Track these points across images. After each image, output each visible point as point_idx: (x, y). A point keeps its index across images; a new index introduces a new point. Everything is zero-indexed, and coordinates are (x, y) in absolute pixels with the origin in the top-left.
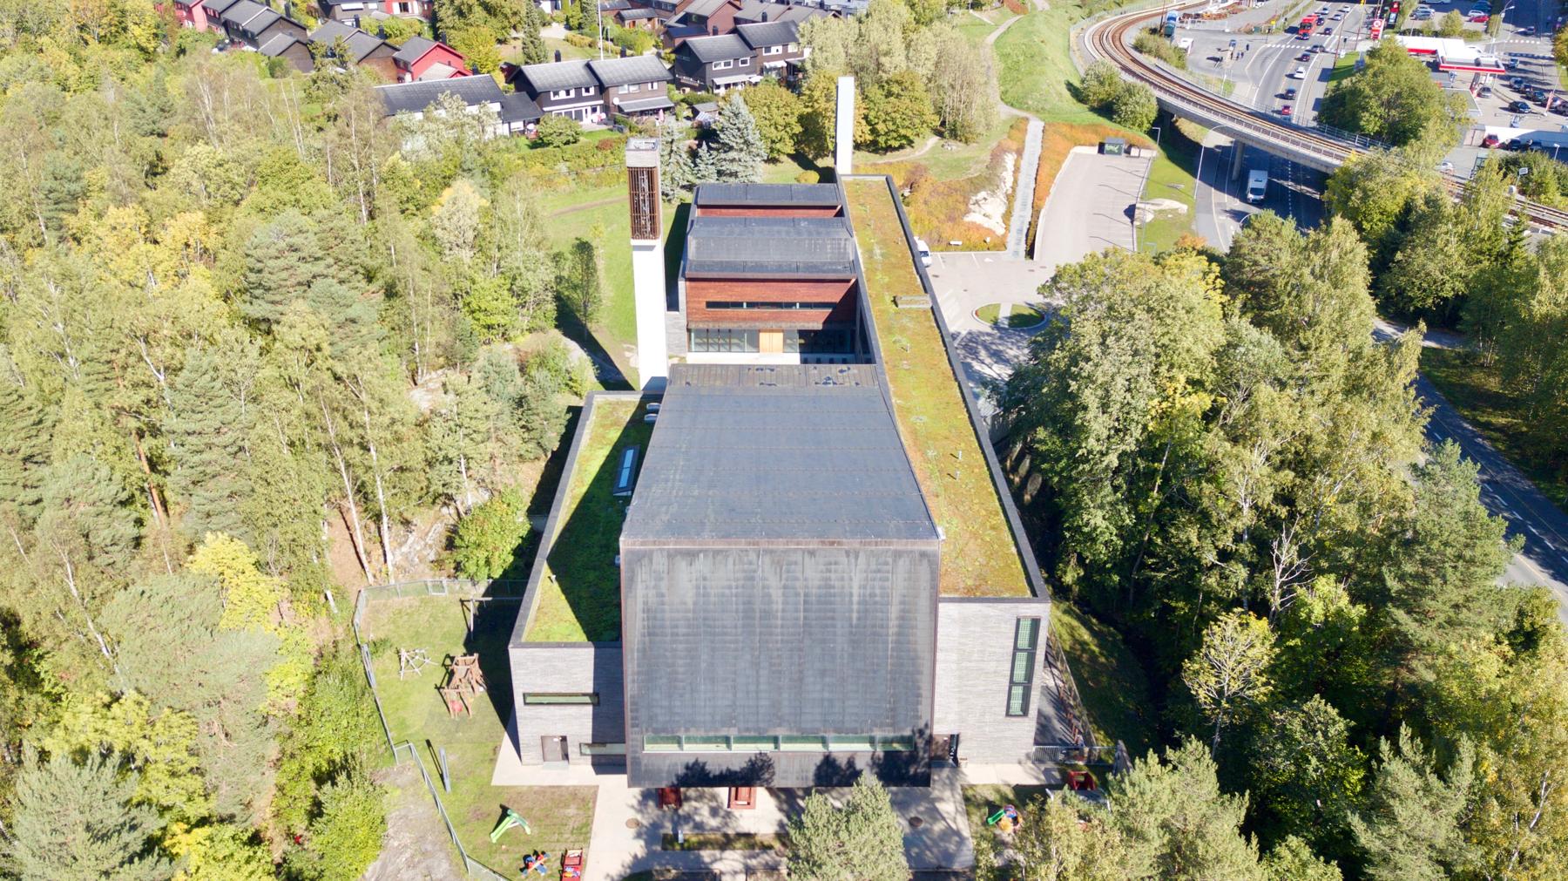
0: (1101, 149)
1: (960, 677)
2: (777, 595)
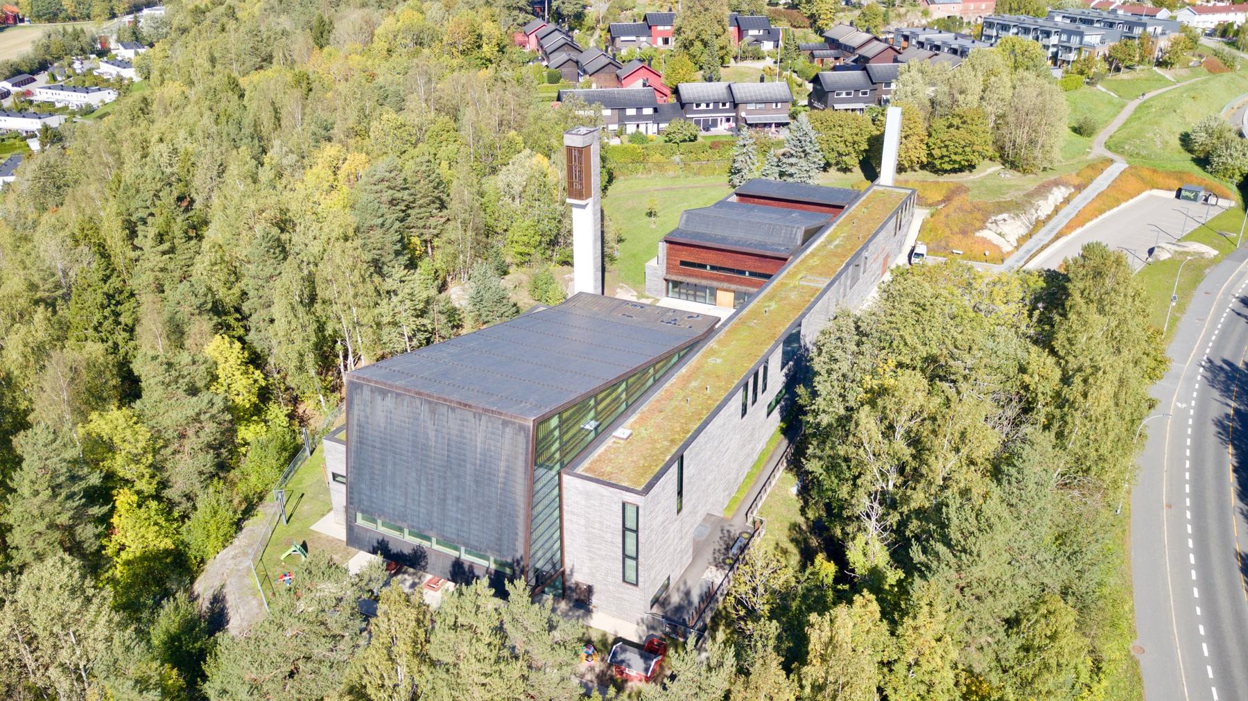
0: (1178, 196)
1: (588, 540)
2: (432, 434)
